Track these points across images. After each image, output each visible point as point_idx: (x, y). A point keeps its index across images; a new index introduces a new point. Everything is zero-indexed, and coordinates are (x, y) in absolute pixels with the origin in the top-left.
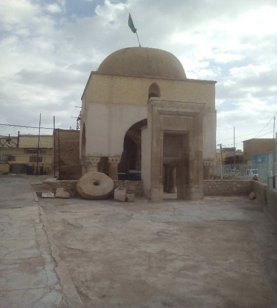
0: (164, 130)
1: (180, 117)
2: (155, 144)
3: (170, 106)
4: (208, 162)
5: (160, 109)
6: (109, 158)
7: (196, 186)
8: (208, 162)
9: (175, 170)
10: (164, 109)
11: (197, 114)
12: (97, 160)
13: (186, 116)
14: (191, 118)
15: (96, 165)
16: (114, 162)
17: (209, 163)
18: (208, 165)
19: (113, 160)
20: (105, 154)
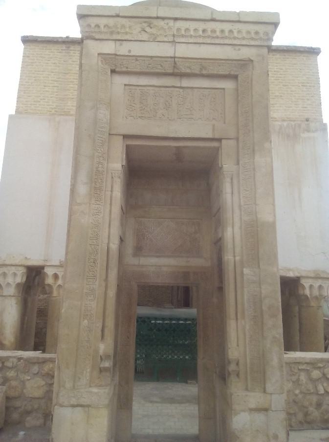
0: (126, 137)
1: (185, 83)
2: (83, 189)
3: (145, 37)
4: (316, 284)
5: (109, 48)
6: (303, 281)
7: (255, 399)
8: (316, 284)
9: (161, 322)
10: (123, 49)
11: (246, 63)
12: (15, 274)
13: (238, 111)
14: (228, 85)
15: (12, 291)
16: (60, 282)
17: (320, 287)
18: (316, 292)
19: (56, 276)
20: (35, 260)
